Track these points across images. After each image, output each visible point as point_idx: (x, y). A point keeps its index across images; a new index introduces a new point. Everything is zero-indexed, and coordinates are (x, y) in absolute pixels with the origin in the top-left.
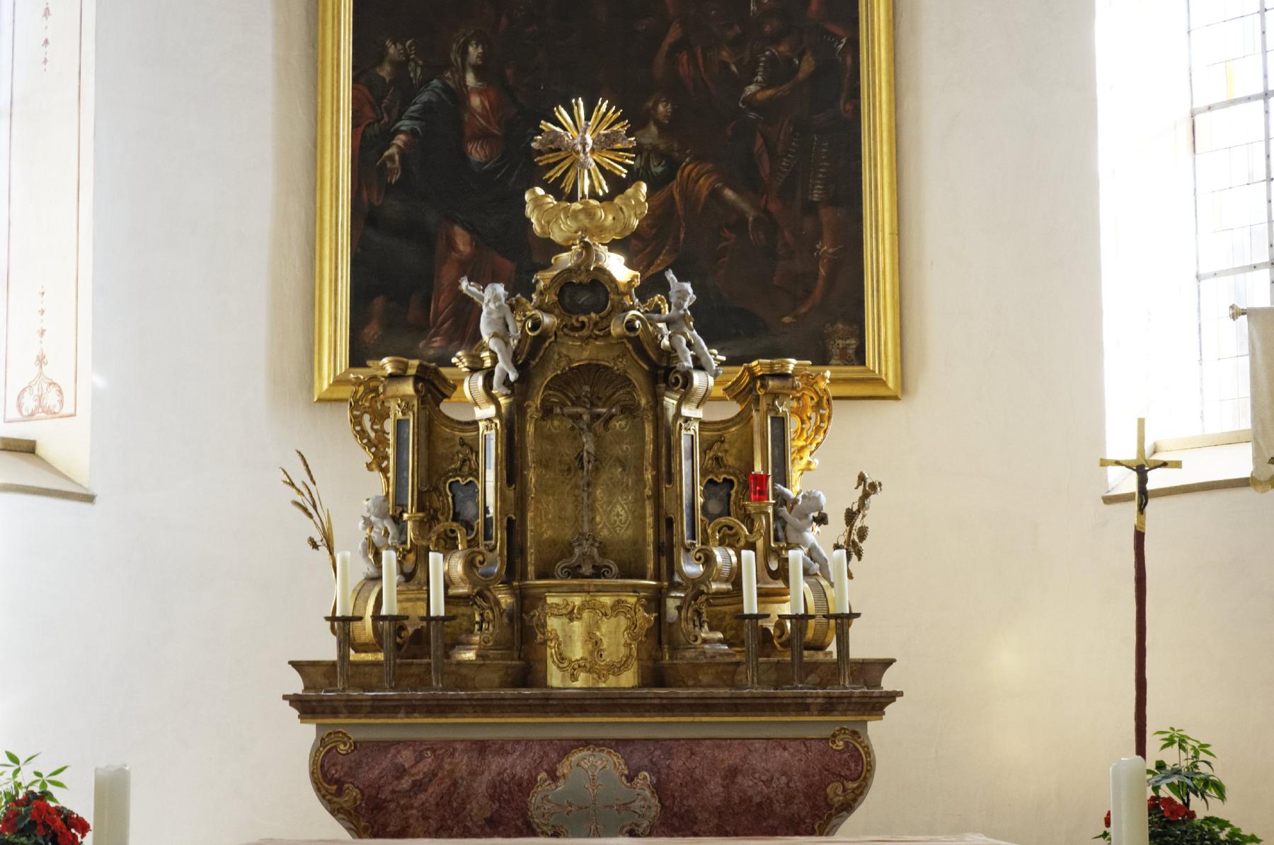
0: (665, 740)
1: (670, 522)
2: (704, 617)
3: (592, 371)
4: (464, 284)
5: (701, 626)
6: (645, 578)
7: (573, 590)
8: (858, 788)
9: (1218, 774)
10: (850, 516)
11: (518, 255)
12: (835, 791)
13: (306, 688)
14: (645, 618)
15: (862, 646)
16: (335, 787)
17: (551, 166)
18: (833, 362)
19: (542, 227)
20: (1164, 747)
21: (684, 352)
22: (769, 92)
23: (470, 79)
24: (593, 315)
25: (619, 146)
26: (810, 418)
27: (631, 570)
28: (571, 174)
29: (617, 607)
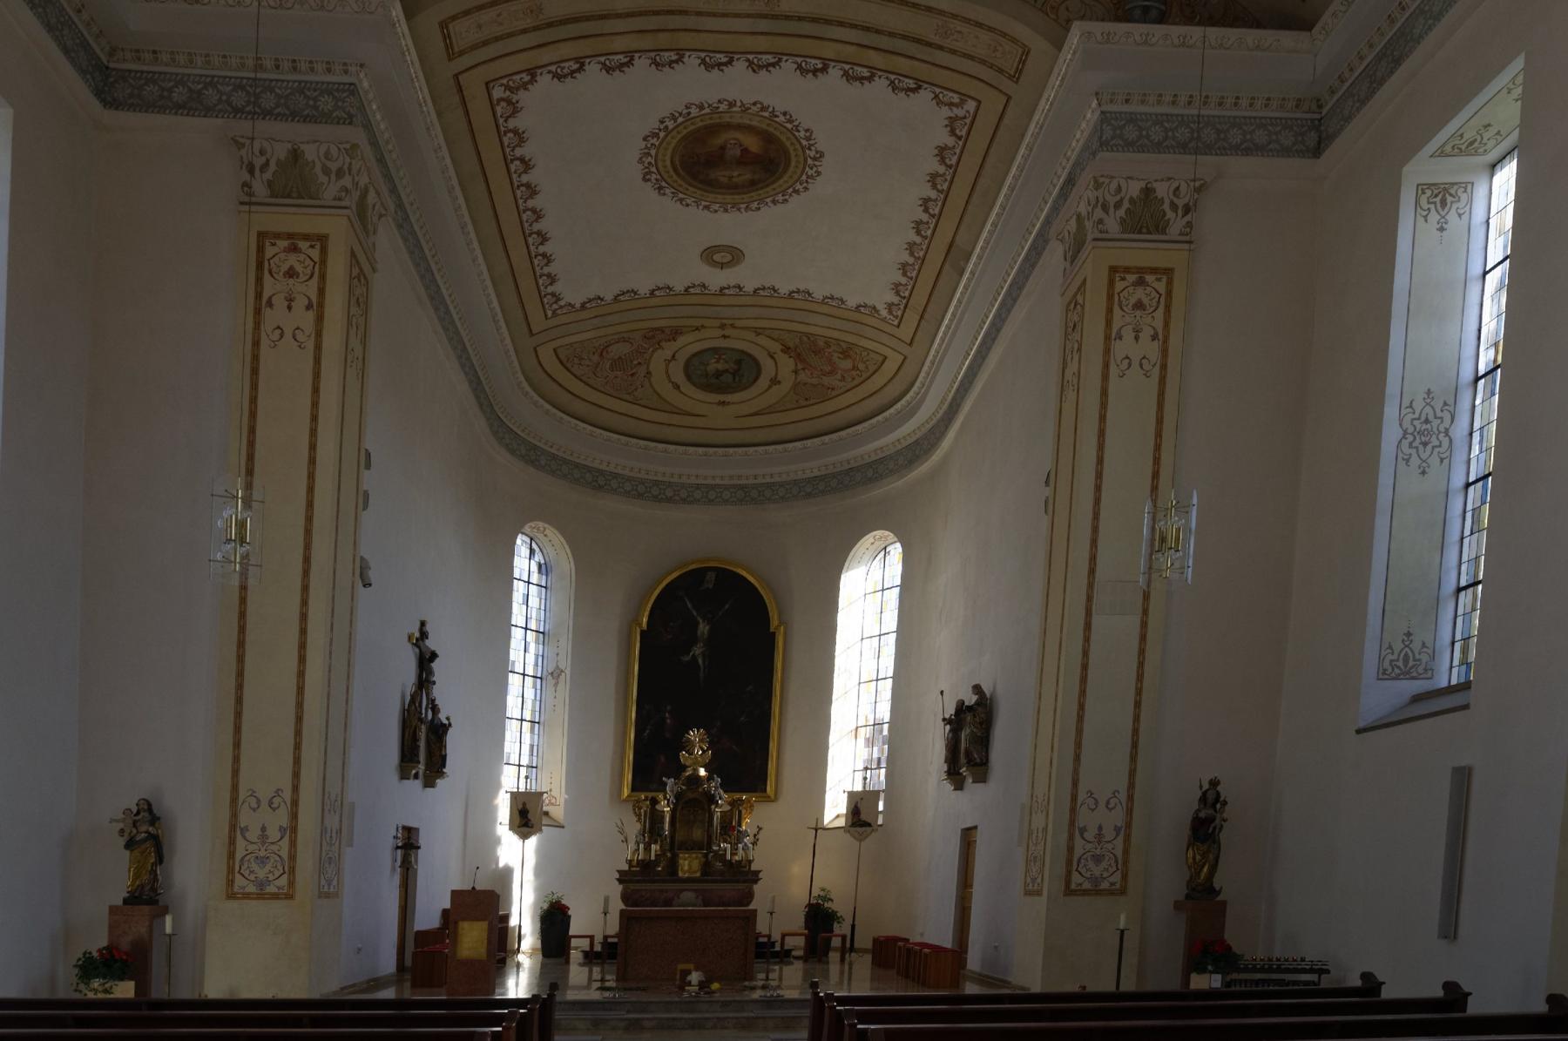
11: (677, 769)
15: (754, 867)
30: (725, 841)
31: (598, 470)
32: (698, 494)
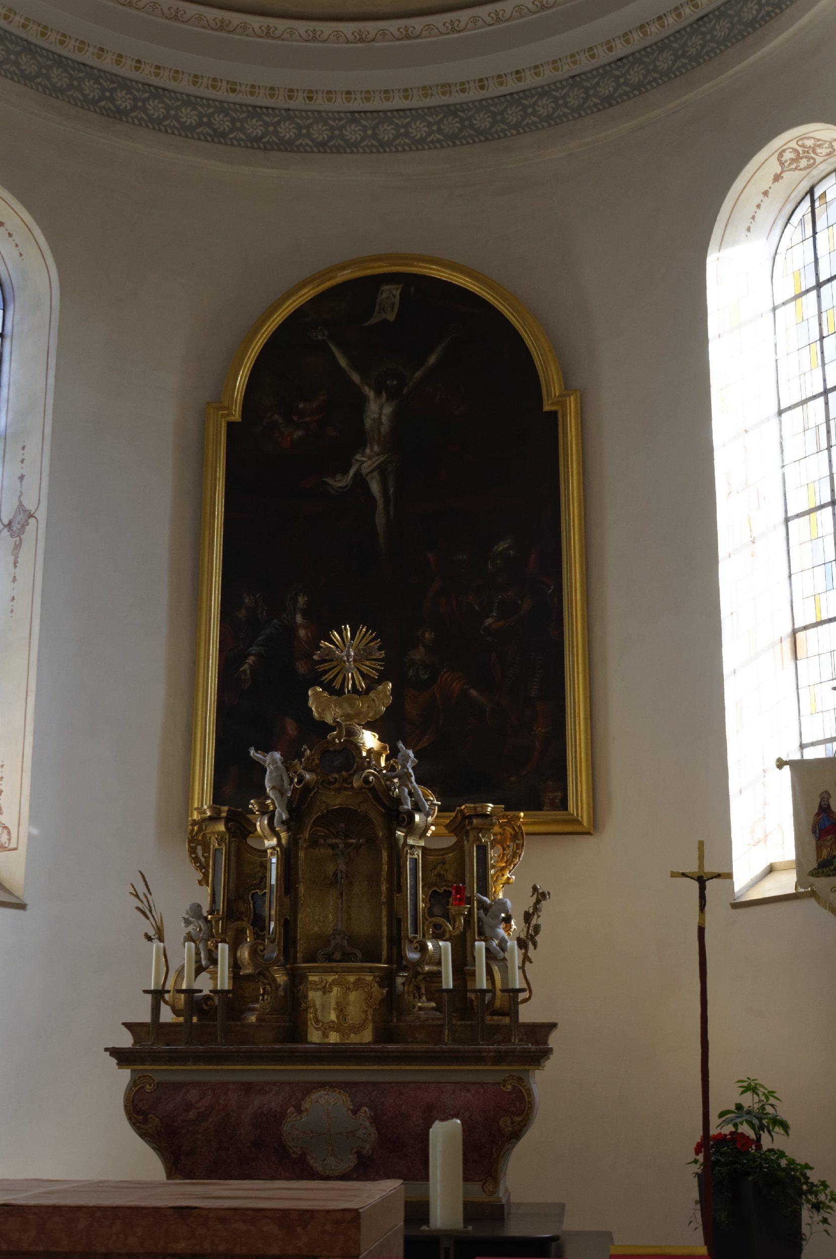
0: (380, 1083)
1: (399, 921)
2: (423, 991)
3: (345, 813)
4: (252, 752)
5: (420, 997)
6: (380, 963)
7: (350, 971)
8: (522, 1121)
9: (782, 1115)
10: (528, 917)
12: (506, 1123)
13: (135, 1043)
14: (378, 992)
15: (527, 1014)
16: (142, 1117)
17: (326, 672)
18: (545, 808)
19: (319, 713)
20: (743, 1093)
21: (406, 799)
22: (500, 623)
23: (299, 619)
24: (344, 773)
25: (373, 657)
26: (509, 846)
27: (372, 956)
28: (340, 677)
29: (358, 984)
30: (439, 935)
31: (114, 77)
32: (353, 133)
